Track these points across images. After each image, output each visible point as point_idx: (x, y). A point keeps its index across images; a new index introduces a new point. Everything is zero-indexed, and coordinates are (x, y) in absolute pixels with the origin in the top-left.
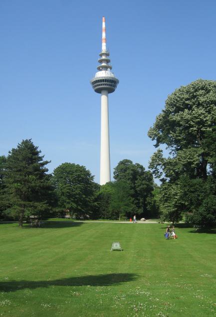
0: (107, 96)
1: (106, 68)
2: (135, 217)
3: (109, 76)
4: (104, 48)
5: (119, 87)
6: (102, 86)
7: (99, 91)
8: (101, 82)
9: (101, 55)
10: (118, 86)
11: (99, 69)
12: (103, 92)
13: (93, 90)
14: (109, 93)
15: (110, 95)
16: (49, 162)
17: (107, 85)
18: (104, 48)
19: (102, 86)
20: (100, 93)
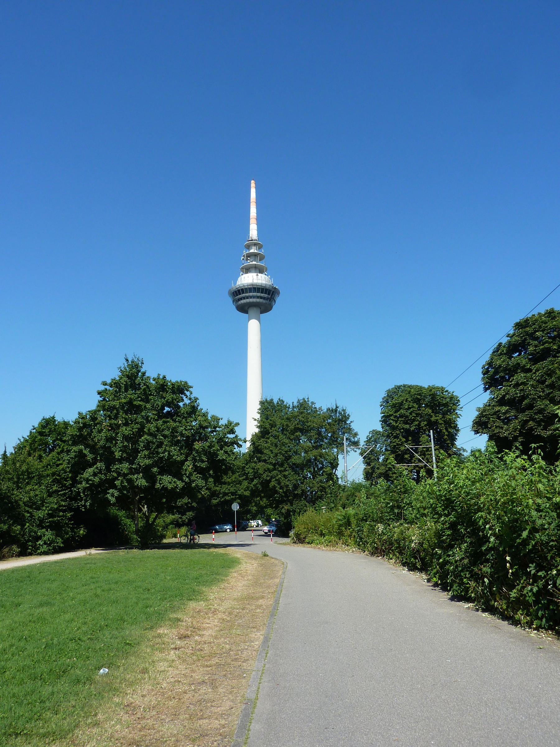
0: (259, 320)
1: (260, 270)
2: (260, 487)
3: (264, 282)
4: (253, 232)
5: (279, 302)
6: (254, 300)
7: (243, 309)
8: (250, 292)
9: (248, 247)
10: (279, 300)
11: (247, 270)
12: (252, 311)
13: (234, 307)
14: (262, 313)
15: (262, 316)
16: (5, 450)
17: (261, 298)
18: (253, 232)
19: (258, 300)
20: (246, 312)
